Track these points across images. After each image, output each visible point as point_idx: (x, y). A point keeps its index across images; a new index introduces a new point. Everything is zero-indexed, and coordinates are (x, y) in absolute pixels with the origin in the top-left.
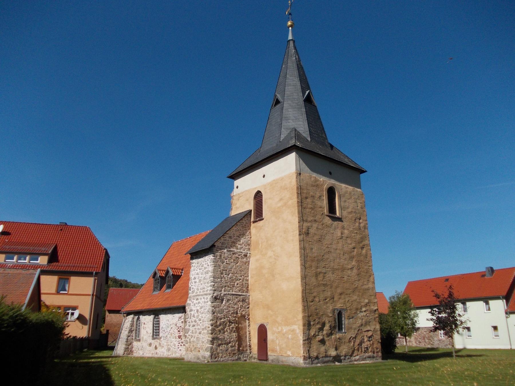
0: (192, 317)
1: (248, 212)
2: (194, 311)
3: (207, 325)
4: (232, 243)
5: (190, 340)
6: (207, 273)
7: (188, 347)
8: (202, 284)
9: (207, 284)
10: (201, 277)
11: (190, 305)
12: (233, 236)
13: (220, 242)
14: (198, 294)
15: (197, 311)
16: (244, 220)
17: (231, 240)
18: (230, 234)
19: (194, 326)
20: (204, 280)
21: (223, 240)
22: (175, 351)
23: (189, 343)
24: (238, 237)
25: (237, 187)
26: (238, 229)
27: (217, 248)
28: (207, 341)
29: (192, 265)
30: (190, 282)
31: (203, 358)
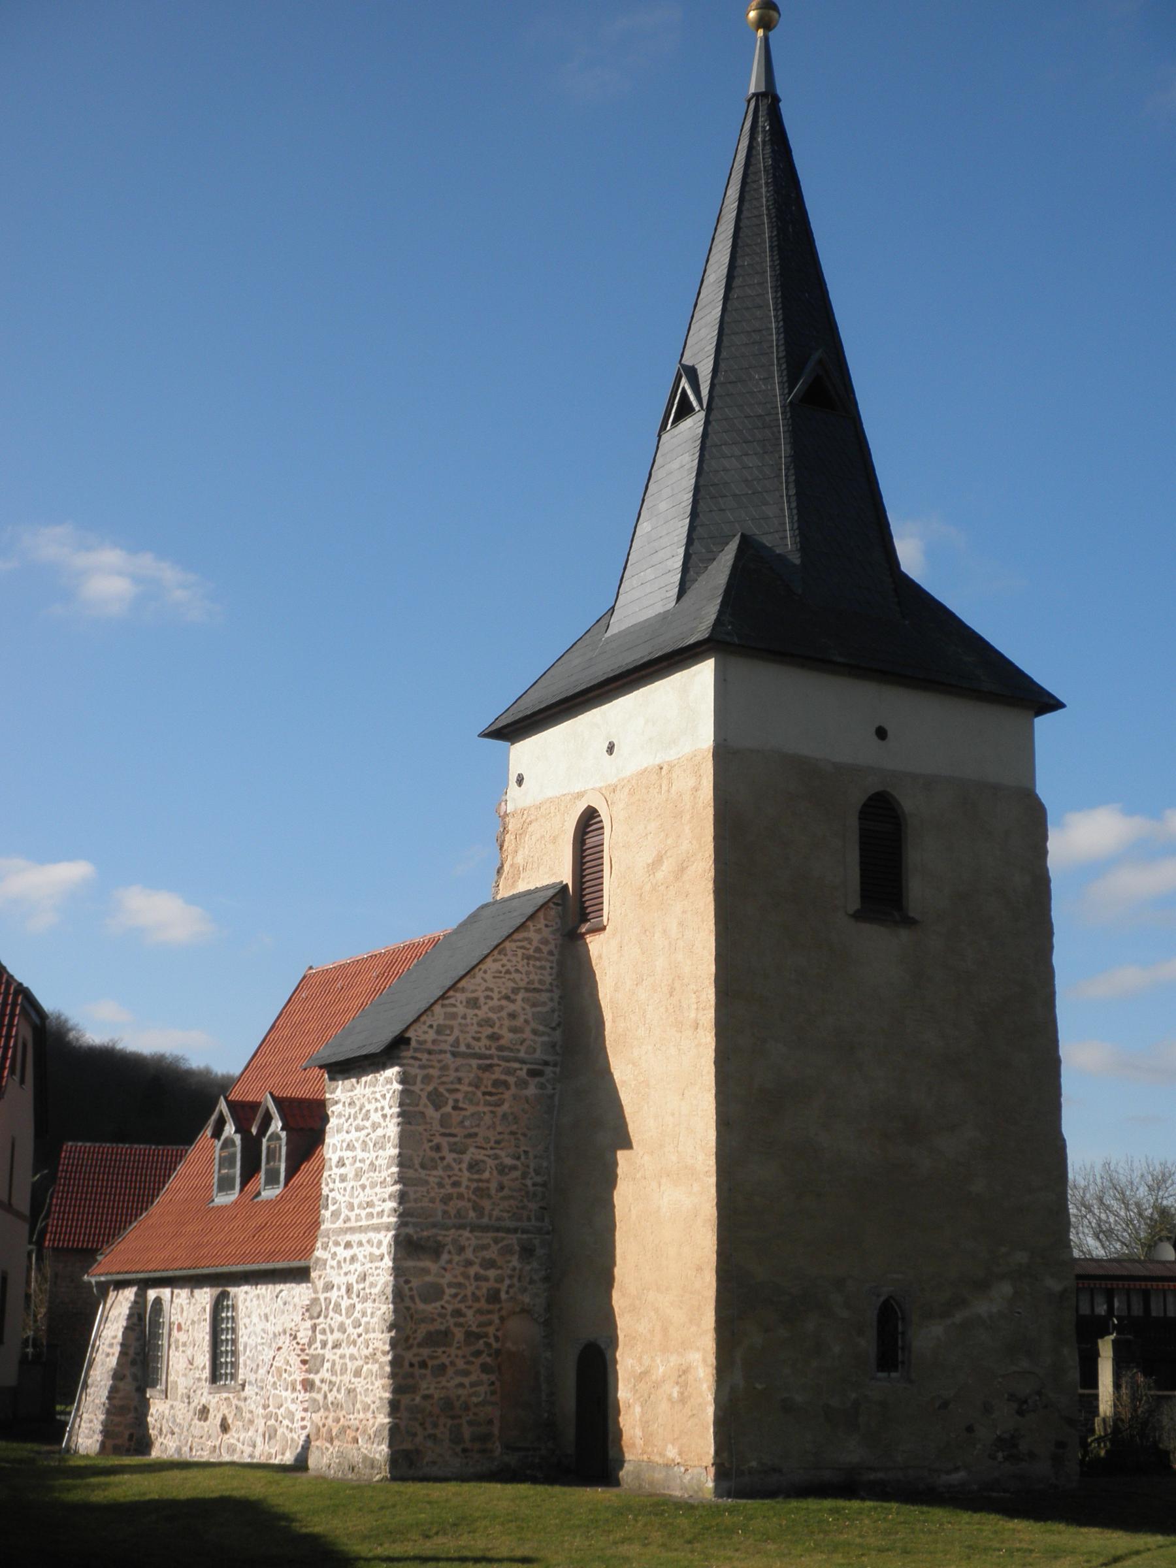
0: (331, 1314)
1: (551, 893)
2: (339, 1289)
3: (379, 1344)
4: (479, 1025)
5: (325, 1397)
6: (379, 1145)
7: (320, 1424)
8: (363, 1187)
9: (381, 1187)
10: (360, 1161)
11: (325, 1264)
12: (488, 997)
13: (428, 1023)
14: (352, 1224)
15: (349, 1290)
16: (532, 928)
17: (476, 1015)
18: (474, 991)
19: (336, 1346)
20: (371, 1174)
21: (442, 1017)
22: (292, 1440)
23: (322, 1410)
24: (507, 998)
25: (520, 781)
26: (509, 965)
27: (416, 1050)
28: (378, 1403)
29: (333, 1108)
30: (326, 1174)
31: (368, 1463)
